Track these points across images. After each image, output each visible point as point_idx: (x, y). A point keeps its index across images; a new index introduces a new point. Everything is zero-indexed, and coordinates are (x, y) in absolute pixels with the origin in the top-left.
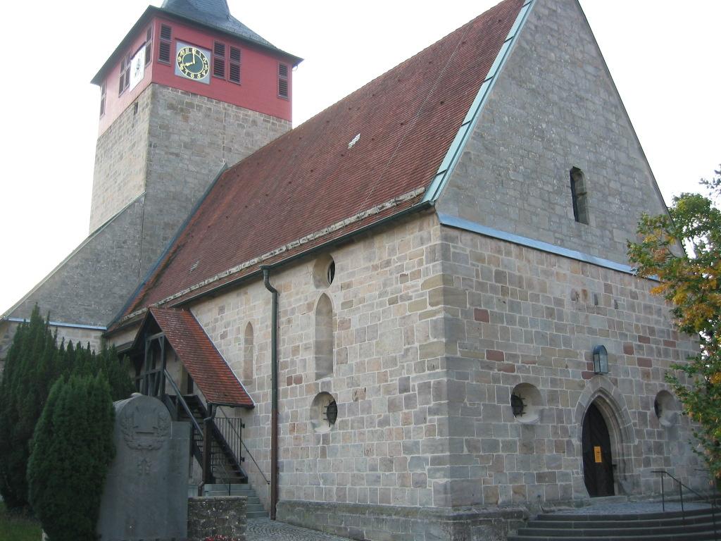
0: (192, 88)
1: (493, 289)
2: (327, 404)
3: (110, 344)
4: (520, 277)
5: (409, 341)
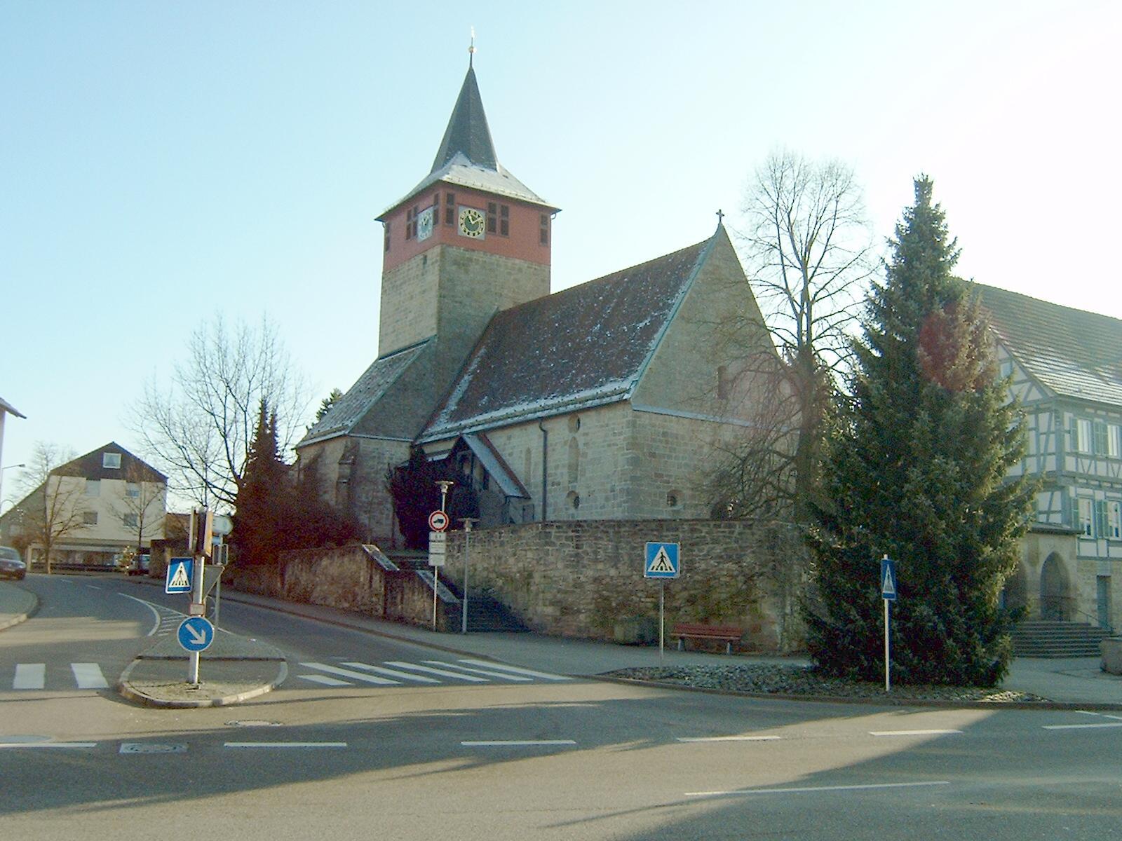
0: (471, 245)
1: (661, 441)
2: (574, 497)
4: (677, 434)
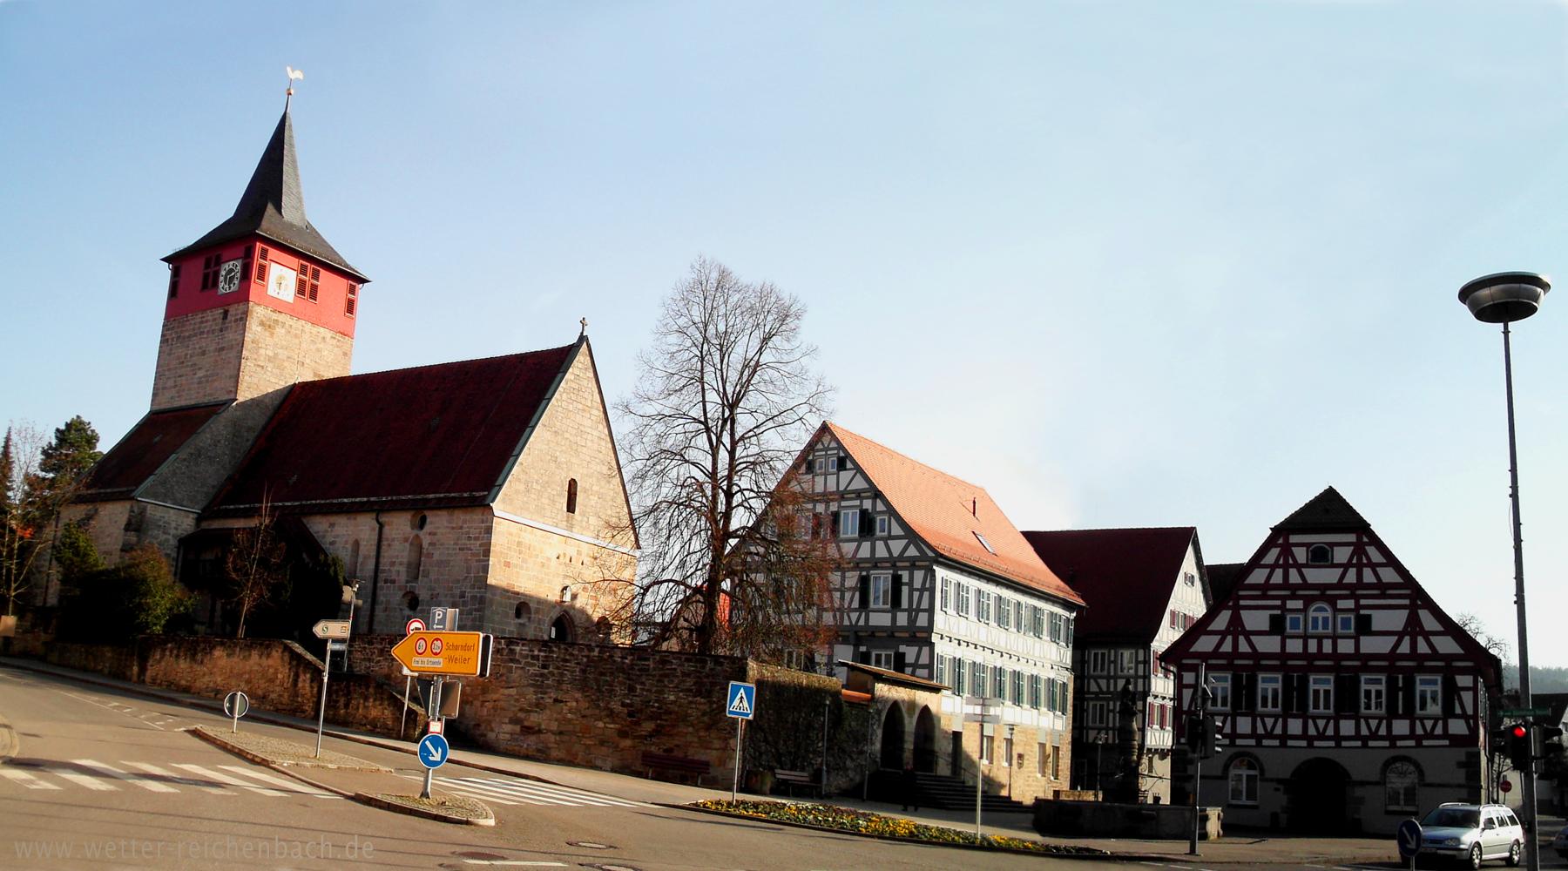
0: (278, 306)
3: (205, 525)
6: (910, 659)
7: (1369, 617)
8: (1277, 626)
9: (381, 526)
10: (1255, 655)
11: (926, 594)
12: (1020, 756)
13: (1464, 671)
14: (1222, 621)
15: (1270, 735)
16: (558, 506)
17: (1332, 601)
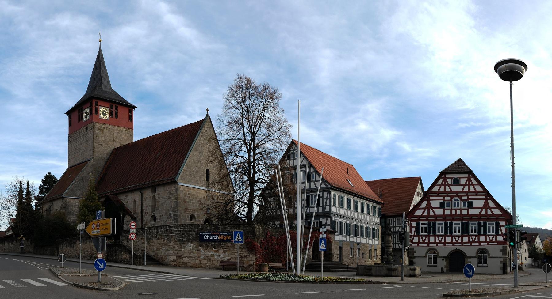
0: (104, 122)
5: (171, 206)
6: (324, 223)
7: (472, 202)
8: (442, 206)
9: (142, 194)
10: (435, 216)
11: (328, 200)
12: (363, 254)
13: (502, 220)
14: (424, 205)
15: (440, 242)
16: (203, 179)
17: (460, 197)
